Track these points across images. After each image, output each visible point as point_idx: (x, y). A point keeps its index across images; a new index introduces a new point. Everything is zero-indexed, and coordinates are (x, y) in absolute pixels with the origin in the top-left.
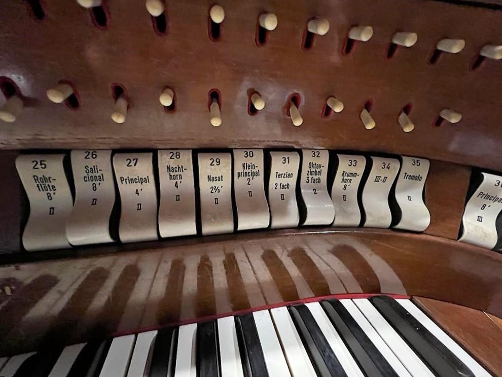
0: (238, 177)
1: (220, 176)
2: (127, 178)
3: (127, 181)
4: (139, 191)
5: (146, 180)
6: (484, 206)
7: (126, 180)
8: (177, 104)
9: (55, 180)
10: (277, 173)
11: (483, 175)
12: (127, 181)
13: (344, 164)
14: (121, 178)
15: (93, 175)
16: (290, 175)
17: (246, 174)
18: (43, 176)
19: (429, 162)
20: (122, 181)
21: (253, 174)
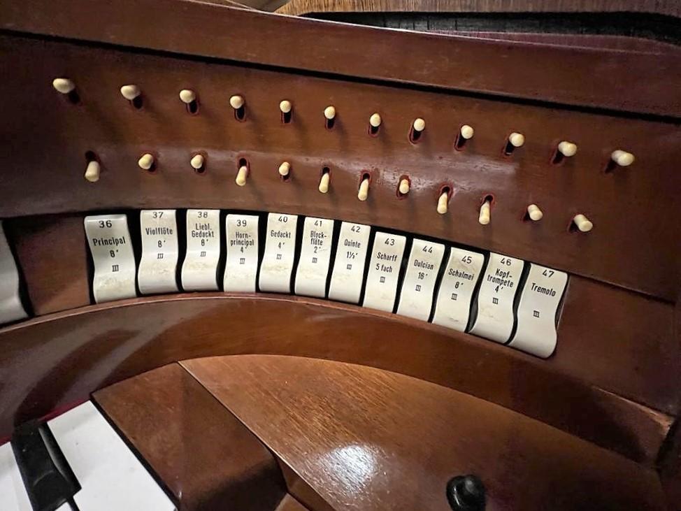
0: (232, 245)
1: (100, 239)
2: (100, 239)
3: (101, 243)
4: (282, 245)
5: (470, 277)
6: (112, 254)
7: (99, 241)
8: (528, 226)
9: (280, 247)
10: (534, 284)
11: (530, 266)
12: (101, 243)
13: (210, 278)
14: (94, 240)
15: (205, 231)
16: (395, 257)
17: (240, 243)
18: (148, 233)
19: (184, 288)
20: (95, 243)
21: (247, 243)
